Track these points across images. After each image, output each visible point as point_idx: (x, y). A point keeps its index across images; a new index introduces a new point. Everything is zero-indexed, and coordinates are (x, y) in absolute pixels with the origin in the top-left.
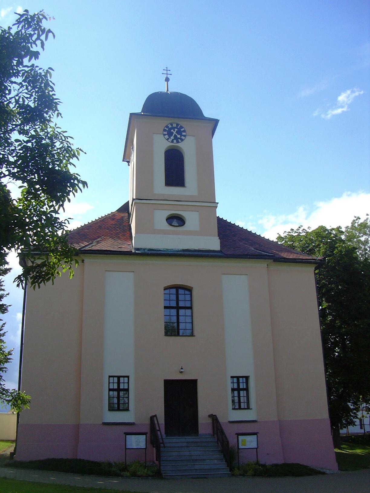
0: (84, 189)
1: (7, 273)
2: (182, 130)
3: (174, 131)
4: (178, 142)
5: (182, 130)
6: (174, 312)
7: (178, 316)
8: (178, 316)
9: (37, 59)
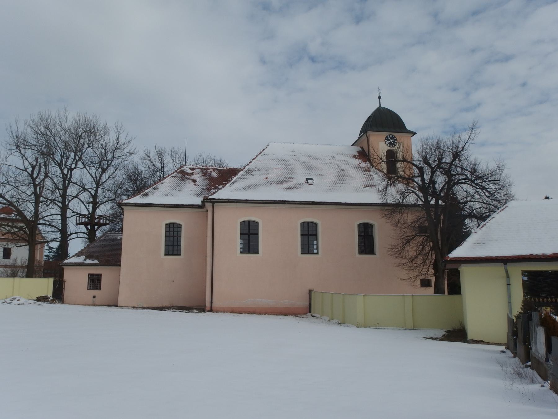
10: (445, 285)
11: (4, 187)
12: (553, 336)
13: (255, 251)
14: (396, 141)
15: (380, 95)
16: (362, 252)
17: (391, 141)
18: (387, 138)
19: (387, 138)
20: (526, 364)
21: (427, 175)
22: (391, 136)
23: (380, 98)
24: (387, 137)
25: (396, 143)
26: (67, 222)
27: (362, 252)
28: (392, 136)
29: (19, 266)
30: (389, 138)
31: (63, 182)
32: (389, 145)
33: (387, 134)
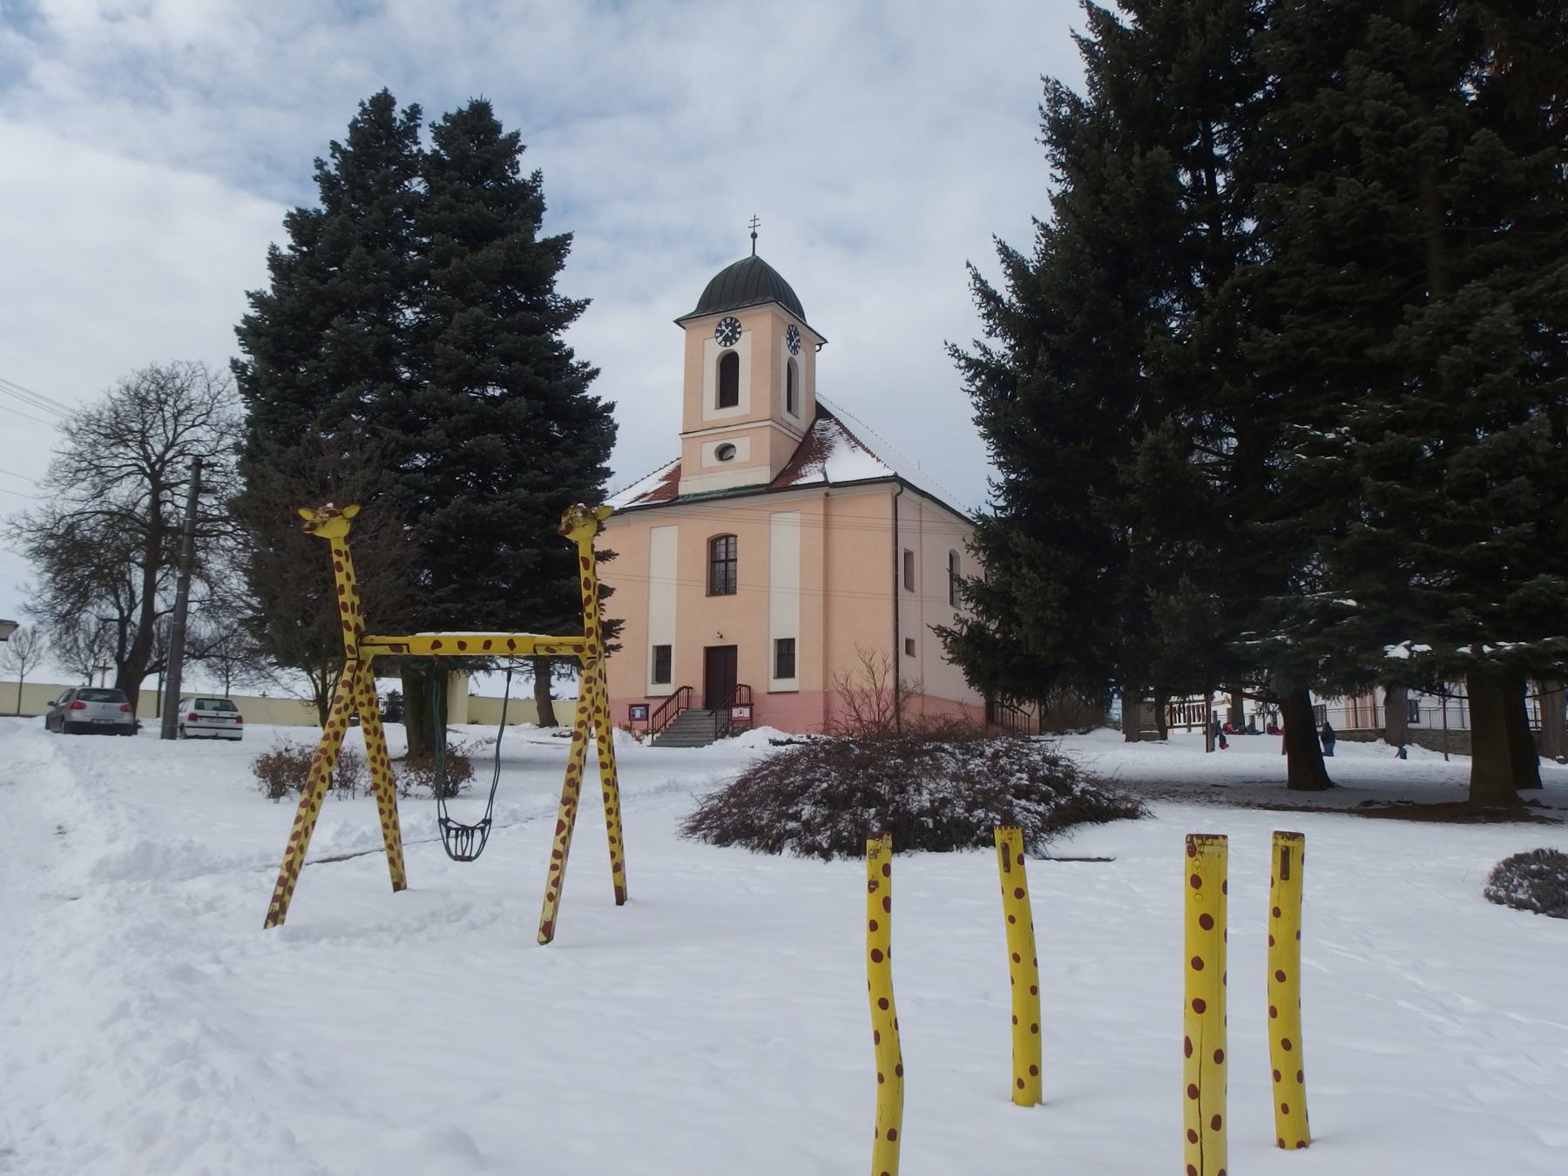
2: (737, 325)
4: (732, 344)
5: (737, 325)
10: (777, 731)
13: (710, 652)
14: (739, 330)
15: (756, 231)
16: (732, 650)
20: (939, 744)
21: (483, 665)
22: (729, 321)
23: (754, 236)
25: (740, 326)
26: (187, 622)
27: (732, 650)
28: (732, 319)
29: (731, 715)
33: (718, 318)
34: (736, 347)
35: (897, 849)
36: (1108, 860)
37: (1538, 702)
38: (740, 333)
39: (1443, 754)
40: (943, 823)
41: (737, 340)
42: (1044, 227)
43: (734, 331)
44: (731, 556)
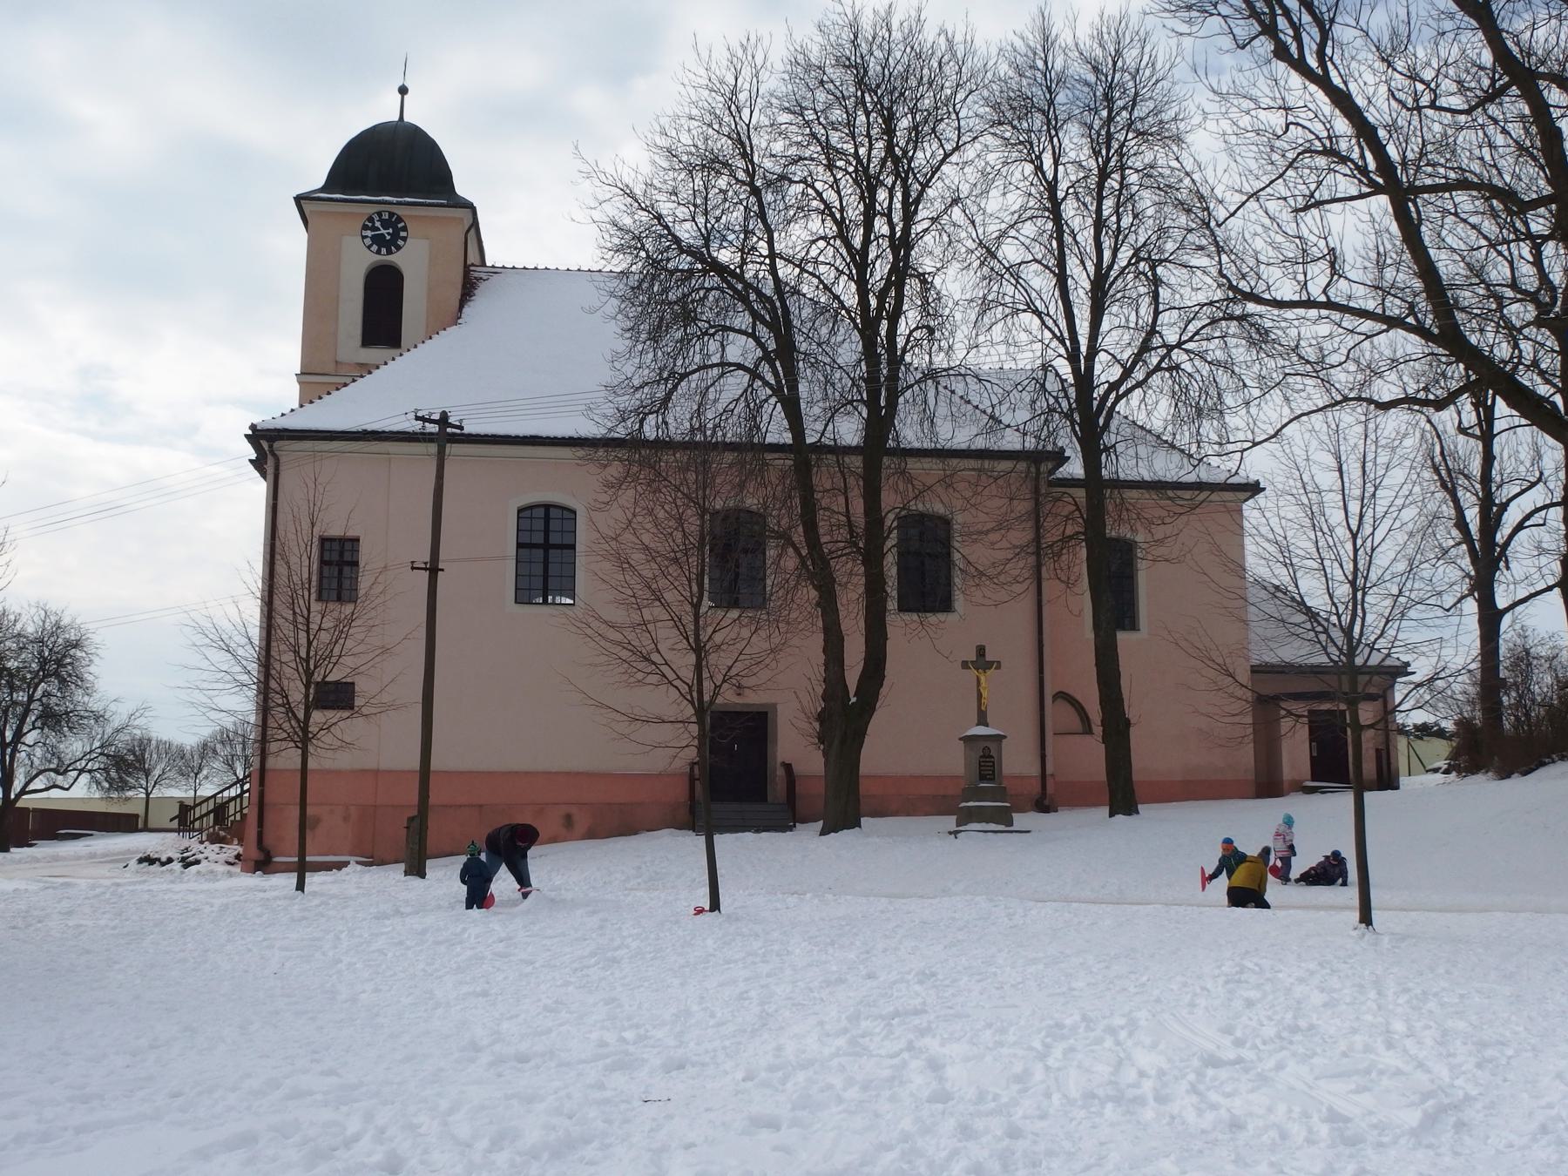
0: (1228, 842)
1: (1301, 875)
2: (400, 226)
3: (388, 234)
4: (389, 252)
5: (400, 226)
6: (555, 539)
7: (547, 531)
8: (547, 531)
9: (250, 432)
11: (1317, 195)
12: (1124, 629)
14: (403, 234)
17: (383, 231)
18: (370, 225)
19: (370, 225)
22: (386, 216)
23: (403, 91)
24: (371, 219)
30: (378, 224)
31: (1380, 142)
32: (375, 248)
34: (396, 258)
35: (1561, 561)
36: (1028, 832)
37: (1398, 680)
38: (404, 239)
39: (177, 813)
40: (1465, 364)
41: (399, 248)
42: (1047, 42)
43: (395, 236)
44: (347, 557)
